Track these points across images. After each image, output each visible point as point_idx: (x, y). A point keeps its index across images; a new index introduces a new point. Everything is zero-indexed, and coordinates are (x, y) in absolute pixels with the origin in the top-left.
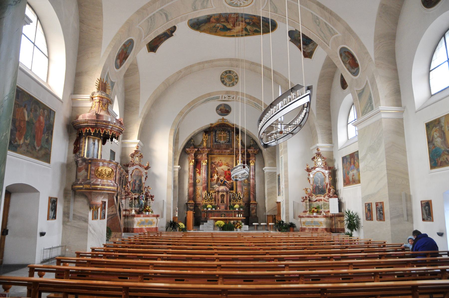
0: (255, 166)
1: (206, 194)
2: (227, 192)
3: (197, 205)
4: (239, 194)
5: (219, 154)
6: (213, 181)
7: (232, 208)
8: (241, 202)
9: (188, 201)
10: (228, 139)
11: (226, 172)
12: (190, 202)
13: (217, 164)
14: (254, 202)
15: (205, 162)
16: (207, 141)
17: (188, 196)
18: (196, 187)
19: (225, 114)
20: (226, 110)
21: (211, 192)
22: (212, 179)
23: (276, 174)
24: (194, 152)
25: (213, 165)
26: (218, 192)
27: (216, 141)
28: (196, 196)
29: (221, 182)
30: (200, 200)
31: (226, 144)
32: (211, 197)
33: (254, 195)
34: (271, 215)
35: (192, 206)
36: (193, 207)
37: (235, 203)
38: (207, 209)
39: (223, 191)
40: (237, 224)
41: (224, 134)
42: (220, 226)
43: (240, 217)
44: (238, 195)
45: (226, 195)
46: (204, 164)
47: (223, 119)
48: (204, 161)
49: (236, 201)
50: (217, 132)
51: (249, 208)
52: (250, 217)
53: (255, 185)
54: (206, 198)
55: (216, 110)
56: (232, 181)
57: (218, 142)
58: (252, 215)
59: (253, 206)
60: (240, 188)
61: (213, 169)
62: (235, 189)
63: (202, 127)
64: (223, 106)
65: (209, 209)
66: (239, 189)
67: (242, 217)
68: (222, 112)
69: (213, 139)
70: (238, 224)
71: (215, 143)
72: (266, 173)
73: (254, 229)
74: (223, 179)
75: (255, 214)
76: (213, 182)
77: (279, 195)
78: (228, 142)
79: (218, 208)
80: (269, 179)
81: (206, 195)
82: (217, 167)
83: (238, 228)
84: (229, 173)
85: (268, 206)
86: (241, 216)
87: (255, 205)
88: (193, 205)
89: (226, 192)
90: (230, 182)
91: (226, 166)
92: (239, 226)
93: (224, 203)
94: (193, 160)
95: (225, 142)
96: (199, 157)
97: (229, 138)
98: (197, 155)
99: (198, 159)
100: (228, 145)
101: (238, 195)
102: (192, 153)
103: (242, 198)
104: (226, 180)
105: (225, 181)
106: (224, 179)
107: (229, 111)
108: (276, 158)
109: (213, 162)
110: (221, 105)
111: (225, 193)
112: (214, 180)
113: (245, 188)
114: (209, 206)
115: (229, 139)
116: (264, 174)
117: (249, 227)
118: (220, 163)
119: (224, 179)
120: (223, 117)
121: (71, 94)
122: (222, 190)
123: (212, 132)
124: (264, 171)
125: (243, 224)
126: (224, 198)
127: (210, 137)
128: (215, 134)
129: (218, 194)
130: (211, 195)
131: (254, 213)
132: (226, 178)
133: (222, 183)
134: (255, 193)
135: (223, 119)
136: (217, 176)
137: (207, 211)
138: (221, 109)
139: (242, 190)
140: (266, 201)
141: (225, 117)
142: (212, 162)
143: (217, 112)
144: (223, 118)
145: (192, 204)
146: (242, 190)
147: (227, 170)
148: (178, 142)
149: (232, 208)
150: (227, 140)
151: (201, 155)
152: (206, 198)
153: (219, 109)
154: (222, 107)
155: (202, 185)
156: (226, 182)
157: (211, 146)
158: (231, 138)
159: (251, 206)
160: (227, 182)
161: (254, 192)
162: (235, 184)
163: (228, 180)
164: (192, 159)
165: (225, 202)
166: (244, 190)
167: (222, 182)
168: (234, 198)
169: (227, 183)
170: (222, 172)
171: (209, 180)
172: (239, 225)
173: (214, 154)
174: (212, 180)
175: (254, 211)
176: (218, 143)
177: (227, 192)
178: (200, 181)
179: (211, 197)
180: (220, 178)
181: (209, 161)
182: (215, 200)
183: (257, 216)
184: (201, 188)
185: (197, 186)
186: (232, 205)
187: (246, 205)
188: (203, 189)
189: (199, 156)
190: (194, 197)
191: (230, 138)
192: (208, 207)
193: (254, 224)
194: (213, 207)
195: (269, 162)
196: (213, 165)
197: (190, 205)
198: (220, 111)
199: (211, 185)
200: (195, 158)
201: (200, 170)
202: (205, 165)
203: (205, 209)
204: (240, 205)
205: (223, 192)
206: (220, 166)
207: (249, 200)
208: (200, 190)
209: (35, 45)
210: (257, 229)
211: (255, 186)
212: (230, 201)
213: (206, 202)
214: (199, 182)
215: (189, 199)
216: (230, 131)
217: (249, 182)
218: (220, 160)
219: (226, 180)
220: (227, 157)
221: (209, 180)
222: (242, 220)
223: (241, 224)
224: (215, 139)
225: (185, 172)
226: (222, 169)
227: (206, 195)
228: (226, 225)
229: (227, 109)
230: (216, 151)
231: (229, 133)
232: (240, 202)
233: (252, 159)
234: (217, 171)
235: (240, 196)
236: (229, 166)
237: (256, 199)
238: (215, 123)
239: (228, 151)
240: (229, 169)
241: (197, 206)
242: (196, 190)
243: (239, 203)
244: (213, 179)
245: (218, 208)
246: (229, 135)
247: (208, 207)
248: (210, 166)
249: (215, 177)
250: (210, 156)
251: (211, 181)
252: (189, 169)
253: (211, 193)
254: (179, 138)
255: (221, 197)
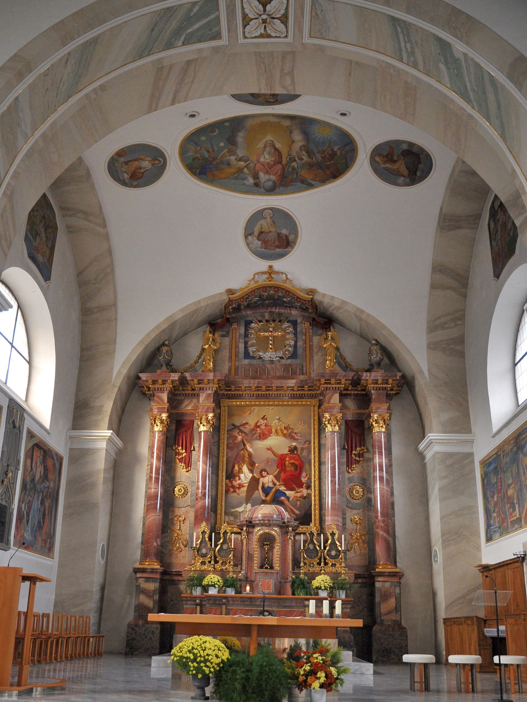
0: (388, 435)
1: (204, 533)
2: (284, 526)
3: (176, 578)
4: (333, 534)
5: (258, 397)
6: (235, 491)
7: (304, 587)
8: (341, 568)
9: (142, 562)
10: (290, 346)
11: (281, 459)
12: (147, 565)
13: (253, 430)
14: (390, 569)
15: (208, 422)
16: (216, 351)
17: (142, 543)
18: (173, 511)
19: (278, 250)
20: (279, 234)
21: (224, 527)
22: (231, 482)
23: (473, 462)
24: (168, 386)
25: (236, 433)
26: (250, 524)
27: (247, 355)
28: (173, 544)
29: (266, 496)
30: (186, 560)
31: (283, 361)
32: (225, 547)
33: (390, 540)
34: (467, 618)
35: (153, 580)
36: (157, 585)
37: (317, 569)
38: (205, 589)
39: (267, 522)
40: (308, 661)
41: (275, 330)
42: (199, 669)
43: (319, 613)
44: (326, 541)
45: (278, 539)
46: (202, 428)
47: (271, 272)
48: (204, 417)
49: (319, 564)
50: (253, 325)
51: (372, 594)
52: (374, 629)
53: (393, 504)
54: (204, 551)
55: (246, 237)
56: (305, 492)
57: (254, 358)
58: (382, 621)
59: (387, 585)
60: (337, 516)
61: (238, 447)
62: (318, 522)
63: (199, 302)
64: (269, 220)
65: (213, 592)
66: (329, 520)
67: (344, 615)
68: (265, 243)
69: (237, 347)
70: (318, 658)
71: (247, 361)
72: (434, 456)
73: (407, 686)
74: (271, 485)
75: (394, 617)
76: (235, 494)
77: (489, 539)
78: (289, 358)
79: (248, 588)
80: (446, 477)
81: (203, 537)
82: (249, 442)
83: (316, 685)
84: (292, 461)
85: (446, 583)
86: (338, 610)
87: (395, 580)
88: (158, 576)
89: (281, 527)
90: (299, 495)
91: (283, 439)
92: (321, 675)
93: (272, 568)
94: (164, 416)
95: (281, 358)
96: (188, 406)
97: (292, 343)
98: (181, 402)
99: (183, 414)
100: (290, 365)
101: (326, 541)
102: (161, 390)
103: (345, 552)
104: (282, 488)
105: (278, 491)
106: (274, 484)
107: (291, 237)
108: (467, 401)
109: (238, 424)
110: (258, 215)
111: (275, 531)
112: (241, 486)
113: (354, 515)
114: (212, 578)
115: (295, 346)
116: (424, 466)
117: (375, 673)
118: (263, 427)
119: (274, 484)
120: (270, 263)
121: (69, 430)
122: (264, 517)
123: (235, 326)
124: (421, 456)
125: (347, 656)
126: (272, 548)
127: (227, 340)
128: (246, 330)
129: (248, 533)
130: (225, 539)
131: (389, 613)
132: (284, 480)
133: (268, 498)
134: (394, 537)
135: (271, 272)
136: (251, 471)
137: (202, 599)
138: (261, 233)
139: (344, 524)
140: (438, 566)
141: (278, 265)
142: (233, 425)
143: (248, 244)
144: (271, 267)
145: (153, 571)
146: (344, 524)
147: (286, 451)
148: (114, 351)
149: (304, 587)
150: (288, 350)
151: (195, 401)
152: (204, 551)
153: (256, 234)
154: (264, 224)
155: (192, 506)
156: (284, 495)
157: (230, 370)
158: (300, 343)
159: (377, 585)
160: (288, 493)
161: (387, 532)
162: (317, 502)
163: (292, 489)
164: (161, 411)
165: (277, 566)
166: (349, 525)
167: (267, 495)
168: (312, 553)
169: (288, 498)
170: (268, 461)
171: (222, 488)
172: (323, 667)
173: (239, 397)
174: (233, 487)
175: (392, 602)
176: (254, 362)
177: (284, 526)
178: (190, 490)
179: (225, 547)
180: (262, 480)
181: (222, 418)
182: (237, 563)
183: (404, 624)
184: (191, 515)
185: (176, 510)
186: (302, 576)
187: (360, 581)
188: (196, 518)
189: (186, 402)
190: (162, 546)
191: (296, 342)
192: (205, 582)
193: (407, 658)
194: (228, 583)
195: (445, 416)
196: (236, 433)
197: (145, 575)
198: (258, 238)
199: (228, 505)
200: (174, 411)
201: (189, 452)
202: (204, 431)
203: (198, 592)
204: (334, 576)
205: (269, 525)
206: (263, 436)
207: (372, 562)
208: (187, 523)
209: (13, 346)
210: (427, 689)
211: (393, 509)
212: (296, 564)
213: (203, 563)
214: (186, 493)
215: (145, 555)
216: (299, 321)
217: (369, 495)
218: (263, 418)
219: (282, 488)
220: (288, 405)
221: (222, 488)
222: (336, 632)
223: (335, 661)
224: (246, 348)
225: (136, 459)
226: (269, 449)
227: (203, 537)
228: (238, 664)
229: (284, 232)
230: (246, 383)
231: (295, 329)
232: (334, 565)
233: (377, 408)
234: (250, 455)
235: (333, 543)
236: (293, 439)
237: (398, 559)
238: (241, 289)
239: (292, 383)
240: (295, 448)
241: (174, 583)
242: (173, 524)
243: (334, 570)
244: (236, 483)
245: (248, 588)
246: (295, 334)
247: (205, 582)
248: (224, 436)
249: (242, 476)
250: (226, 402)
251: (227, 491)
252: (151, 448)
253: (222, 531)
254: (115, 338)
255: (262, 546)
